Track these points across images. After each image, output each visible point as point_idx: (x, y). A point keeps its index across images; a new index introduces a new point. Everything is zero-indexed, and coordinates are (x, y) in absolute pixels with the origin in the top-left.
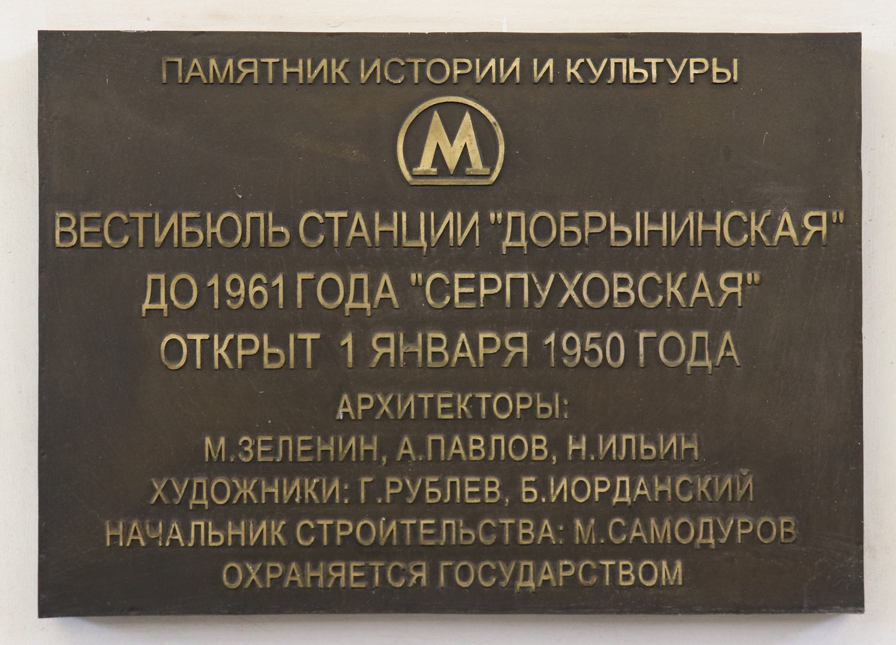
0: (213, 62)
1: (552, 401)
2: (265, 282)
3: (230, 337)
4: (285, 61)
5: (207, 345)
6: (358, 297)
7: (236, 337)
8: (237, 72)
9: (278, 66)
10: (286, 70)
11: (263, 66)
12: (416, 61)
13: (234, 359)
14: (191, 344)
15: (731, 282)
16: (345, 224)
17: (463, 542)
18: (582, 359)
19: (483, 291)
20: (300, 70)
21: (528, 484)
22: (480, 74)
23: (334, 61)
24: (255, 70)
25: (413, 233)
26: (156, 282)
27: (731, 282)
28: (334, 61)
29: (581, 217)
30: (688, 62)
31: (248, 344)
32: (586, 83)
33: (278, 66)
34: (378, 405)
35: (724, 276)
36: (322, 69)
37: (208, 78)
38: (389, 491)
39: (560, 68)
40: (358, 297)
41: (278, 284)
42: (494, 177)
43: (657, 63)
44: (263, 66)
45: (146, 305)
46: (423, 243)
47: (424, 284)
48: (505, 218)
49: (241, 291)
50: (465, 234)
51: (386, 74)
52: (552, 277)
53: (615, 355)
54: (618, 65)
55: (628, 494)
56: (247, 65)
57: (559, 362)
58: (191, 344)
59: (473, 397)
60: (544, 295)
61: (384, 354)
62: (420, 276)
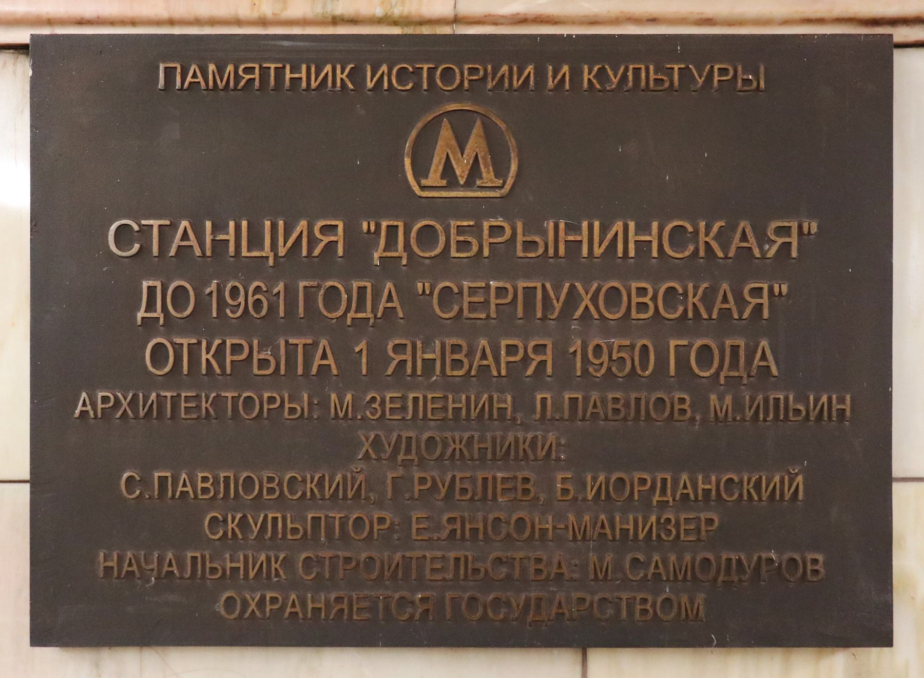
0: (212, 67)
1: (300, 400)
2: (265, 289)
3: (217, 342)
4: (288, 68)
5: (194, 350)
6: (361, 307)
7: (224, 342)
8: (237, 78)
9: (280, 72)
10: (288, 76)
11: (264, 71)
12: (425, 67)
13: (222, 366)
14: (178, 348)
15: (757, 292)
16: (165, 233)
17: (685, 538)
18: (609, 369)
19: (493, 301)
20: (303, 75)
21: (564, 480)
22: (518, 81)
23: (339, 67)
24: (257, 75)
25: (255, 241)
26: (152, 290)
27: (757, 292)
28: (339, 67)
29: (478, 228)
30: (712, 67)
31: (236, 348)
32: (603, 91)
33: (280, 72)
34: (117, 402)
35: (748, 287)
36: (327, 74)
37: (207, 84)
38: (417, 488)
39: (576, 74)
40: (361, 307)
41: (279, 292)
42: (508, 187)
43: (276, 68)
44: (264, 71)
45: (141, 314)
46: (267, 251)
47: (431, 293)
48: (378, 226)
49: (241, 299)
50: (289, 244)
51: (394, 82)
52: (567, 285)
53: (644, 365)
54: (637, 71)
55: (669, 492)
56: (248, 70)
57: (585, 371)
58: (178, 348)
59: (218, 396)
60: (558, 306)
61: (541, 361)
62: (427, 285)
